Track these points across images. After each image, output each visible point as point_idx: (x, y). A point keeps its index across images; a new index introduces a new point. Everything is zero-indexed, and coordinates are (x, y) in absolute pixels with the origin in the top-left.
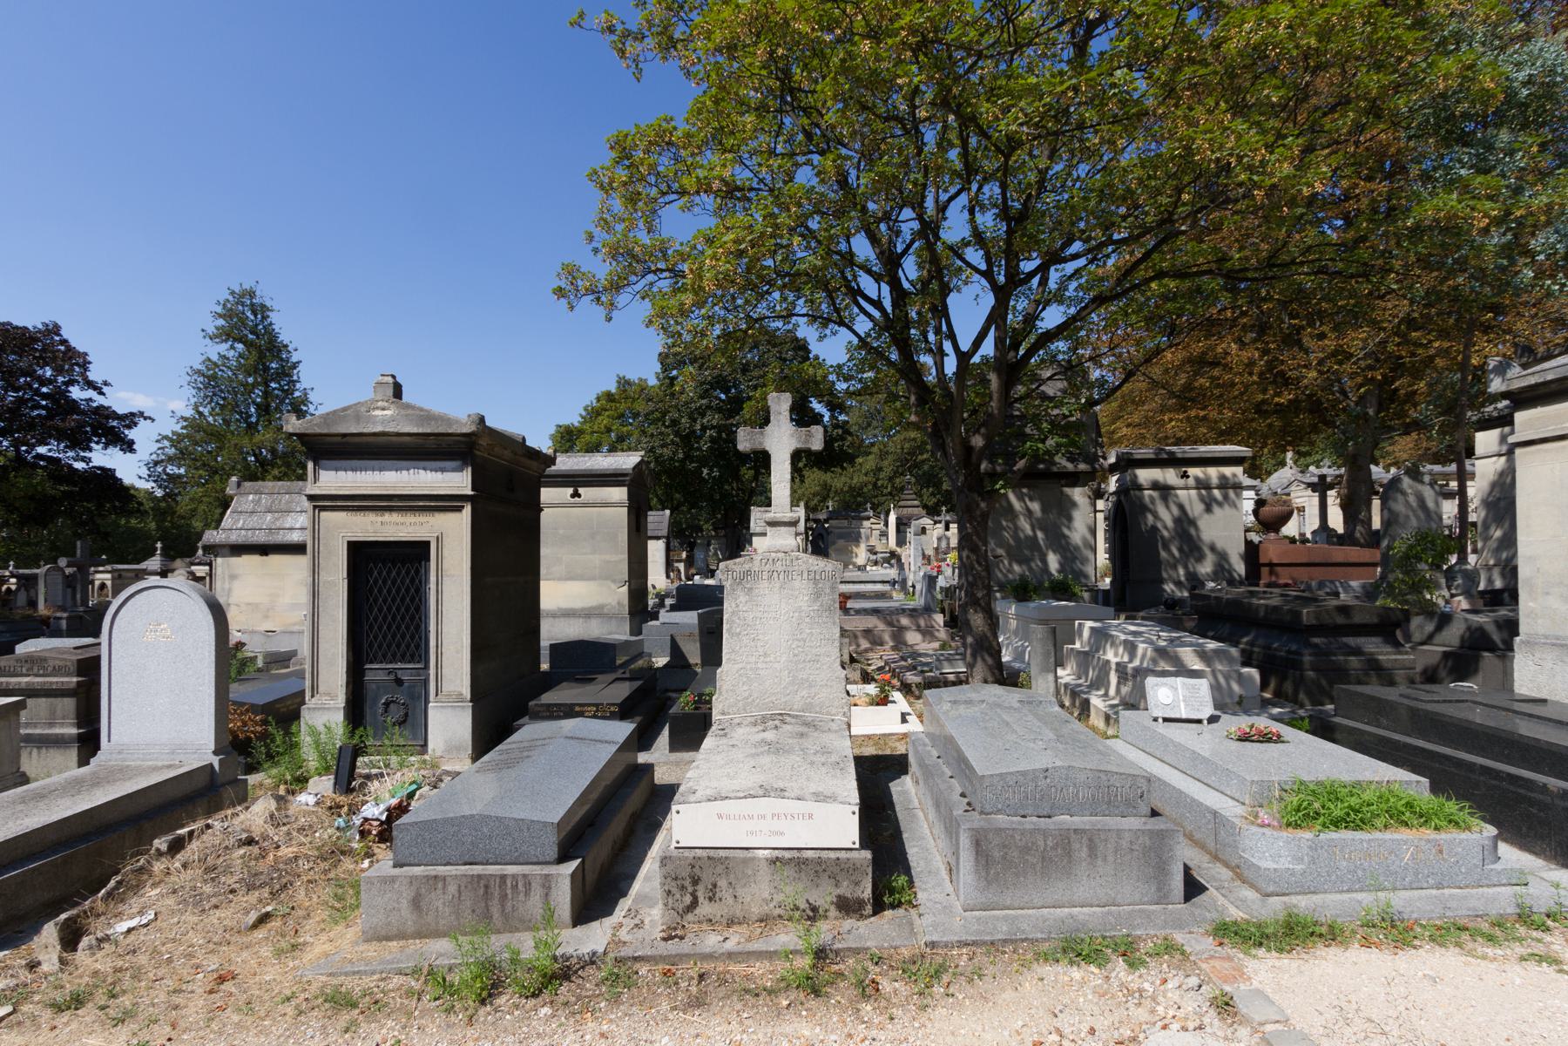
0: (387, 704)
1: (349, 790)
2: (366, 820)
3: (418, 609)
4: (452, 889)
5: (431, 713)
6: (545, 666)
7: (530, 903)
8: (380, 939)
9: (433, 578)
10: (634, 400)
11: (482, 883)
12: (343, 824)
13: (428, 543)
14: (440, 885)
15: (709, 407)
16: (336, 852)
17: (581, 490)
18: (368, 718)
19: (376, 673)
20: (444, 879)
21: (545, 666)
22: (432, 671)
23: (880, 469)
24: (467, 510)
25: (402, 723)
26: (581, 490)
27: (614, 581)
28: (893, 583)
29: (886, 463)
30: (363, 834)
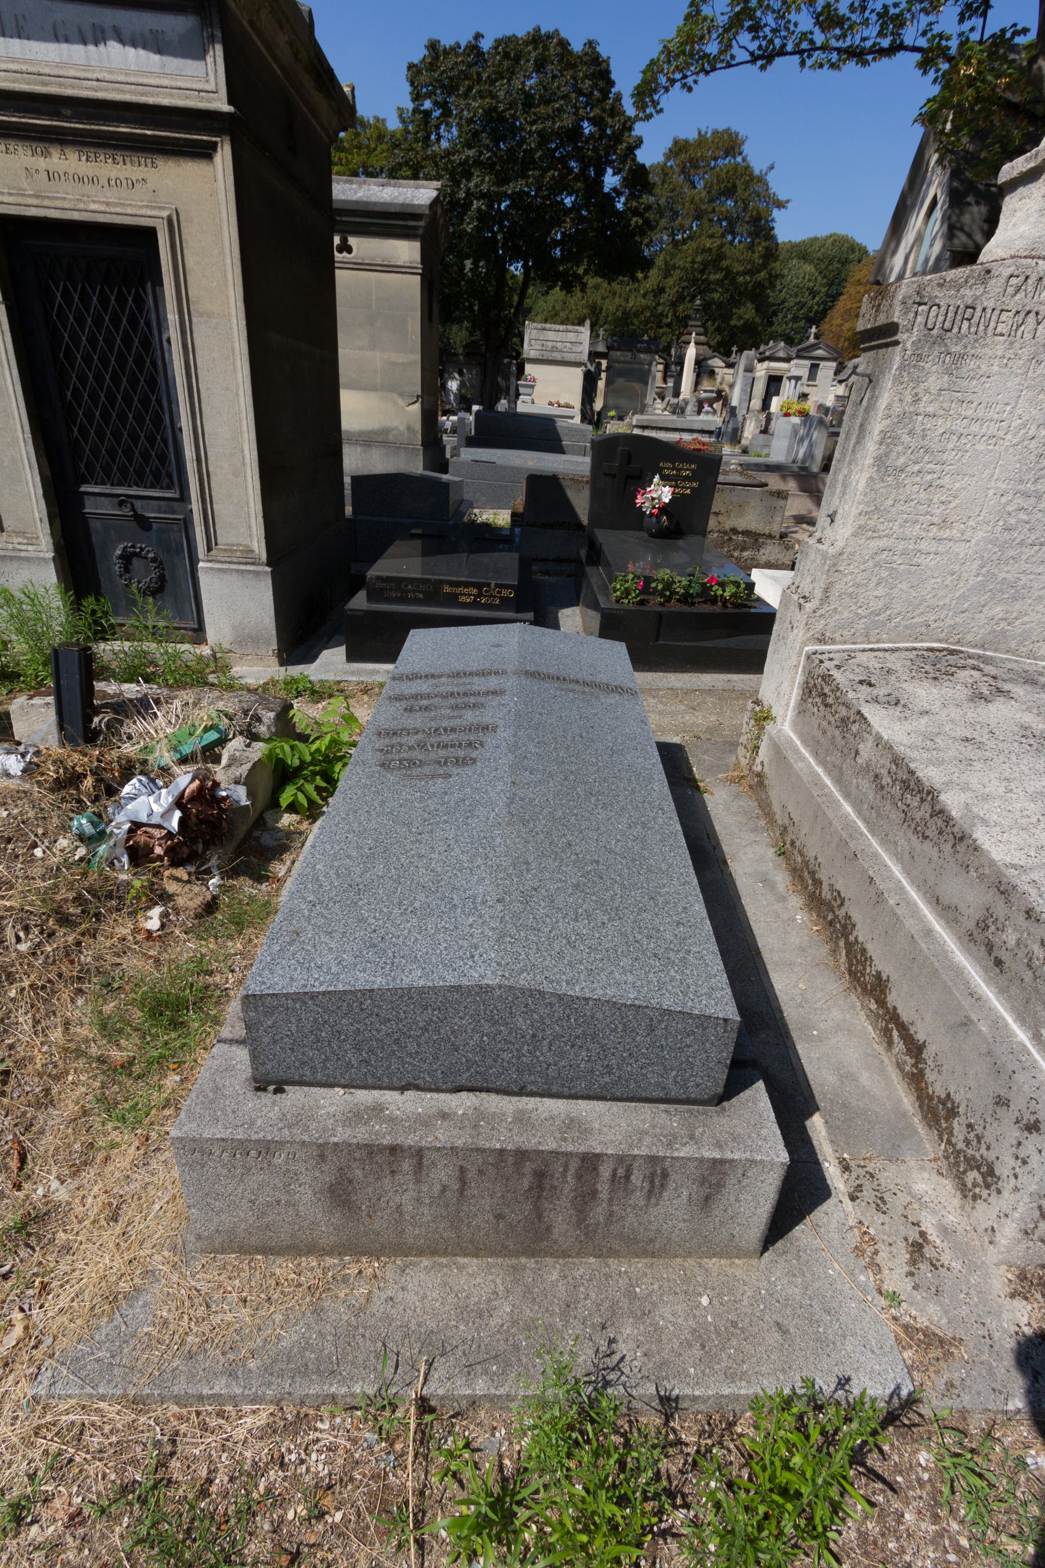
0: (127, 558)
1: (91, 737)
2: (136, 826)
3: (152, 383)
4: (442, 1174)
5: (204, 579)
6: (349, 510)
7: (656, 1212)
8: (245, 1250)
9: (172, 317)
10: (371, 151)
11: (528, 1167)
12: (89, 829)
13: (150, 233)
14: (407, 1165)
15: (478, 163)
16: (89, 905)
17: (352, 241)
18: (104, 583)
19: (100, 500)
20: (419, 1153)
21: (349, 510)
22: (195, 506)
23: (662, 290)
24: (224, 156)
25: (157, 590)
26: (352, 241)
27: (402, 395)
28: (718, 433)
29: (670, 281)
30: (139, 855)
